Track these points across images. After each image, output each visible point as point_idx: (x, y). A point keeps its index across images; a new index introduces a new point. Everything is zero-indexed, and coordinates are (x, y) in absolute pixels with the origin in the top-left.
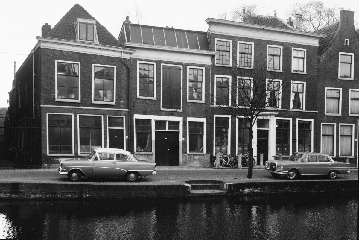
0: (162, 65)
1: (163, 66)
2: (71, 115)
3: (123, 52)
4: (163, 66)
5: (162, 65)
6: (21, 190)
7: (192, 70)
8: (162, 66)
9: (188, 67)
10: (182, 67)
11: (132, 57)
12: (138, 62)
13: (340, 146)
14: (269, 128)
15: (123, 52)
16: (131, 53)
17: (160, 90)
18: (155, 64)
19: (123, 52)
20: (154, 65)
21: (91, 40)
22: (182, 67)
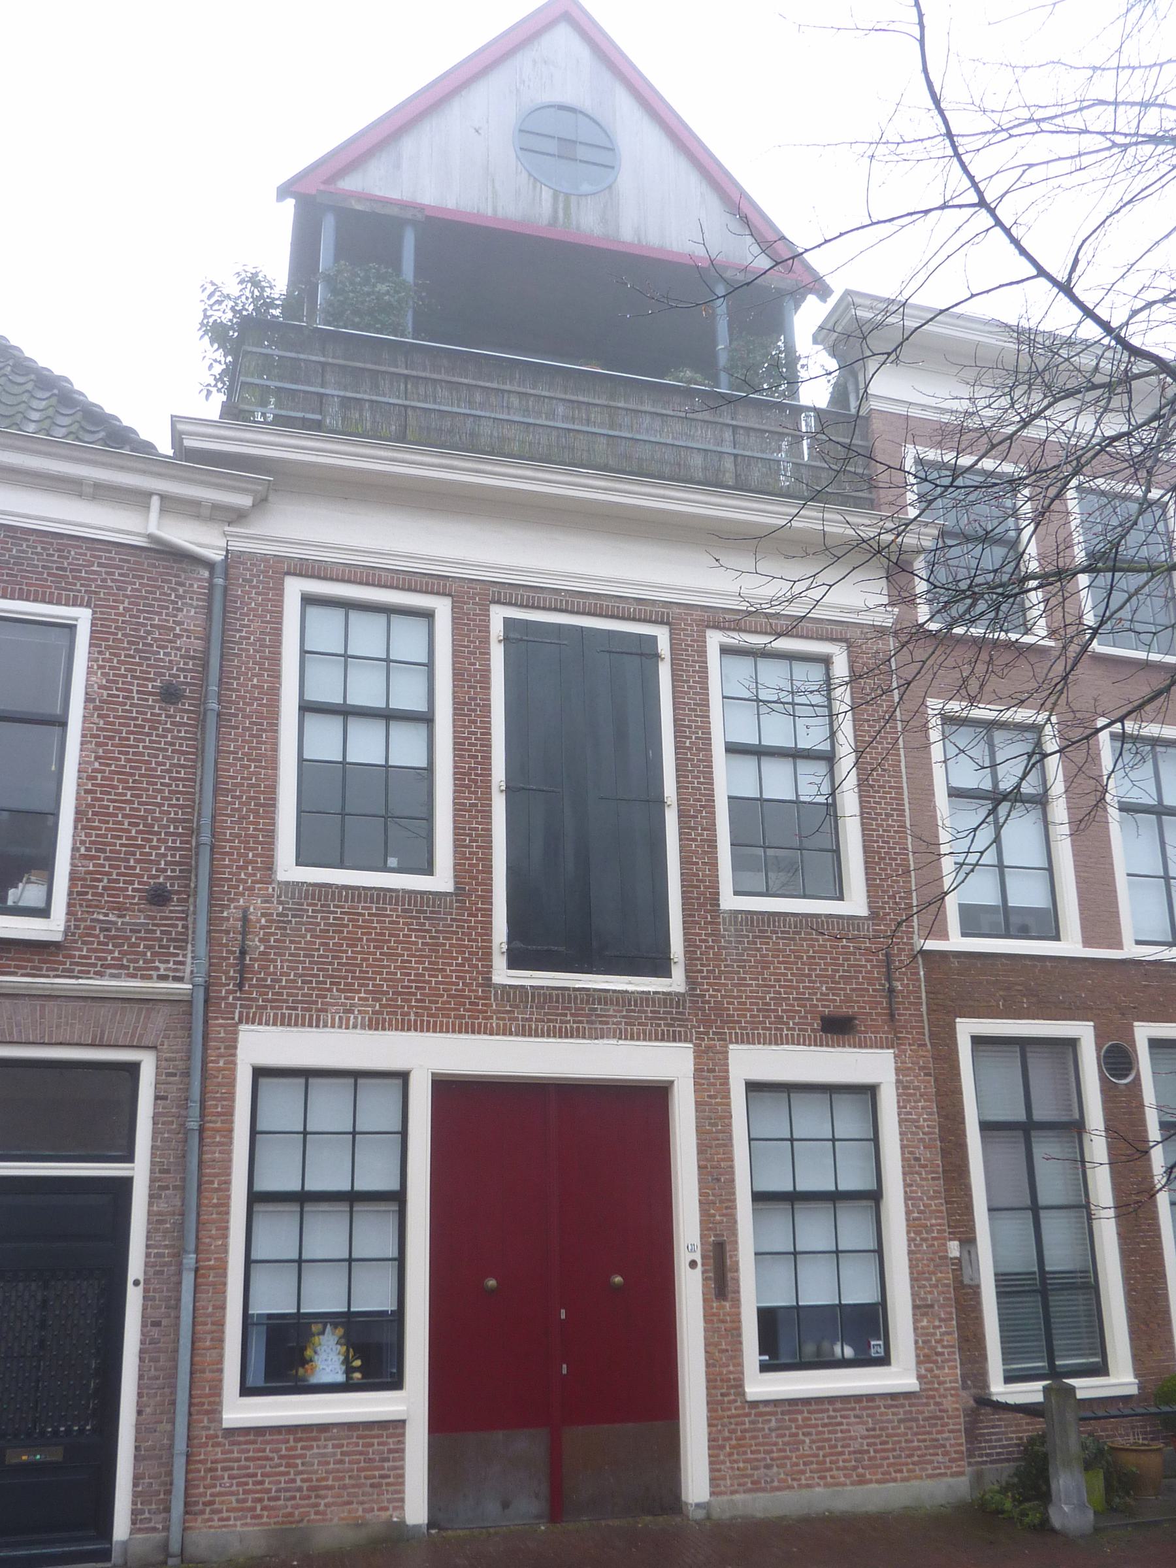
0: (498, 615)
1: (508, 622)
2: (133, 1069)
3: (155, 502)
4: (508, 622)
5: (498, 615)
6: (141, 1471)
7: (745, 665)
8: (497, 628)
9: (715, 639)
10: (662, 634)
11: (237, 545)
12: (294, 588)
13: (604, 996)
14: (403, 1077)
15: (155, 502)
16: (237, 516)
17: (487, 815)
18: (442, 608)
19: (163, 497)
20: (428, 615)
21: (759, 890)
22: (662, 634)
